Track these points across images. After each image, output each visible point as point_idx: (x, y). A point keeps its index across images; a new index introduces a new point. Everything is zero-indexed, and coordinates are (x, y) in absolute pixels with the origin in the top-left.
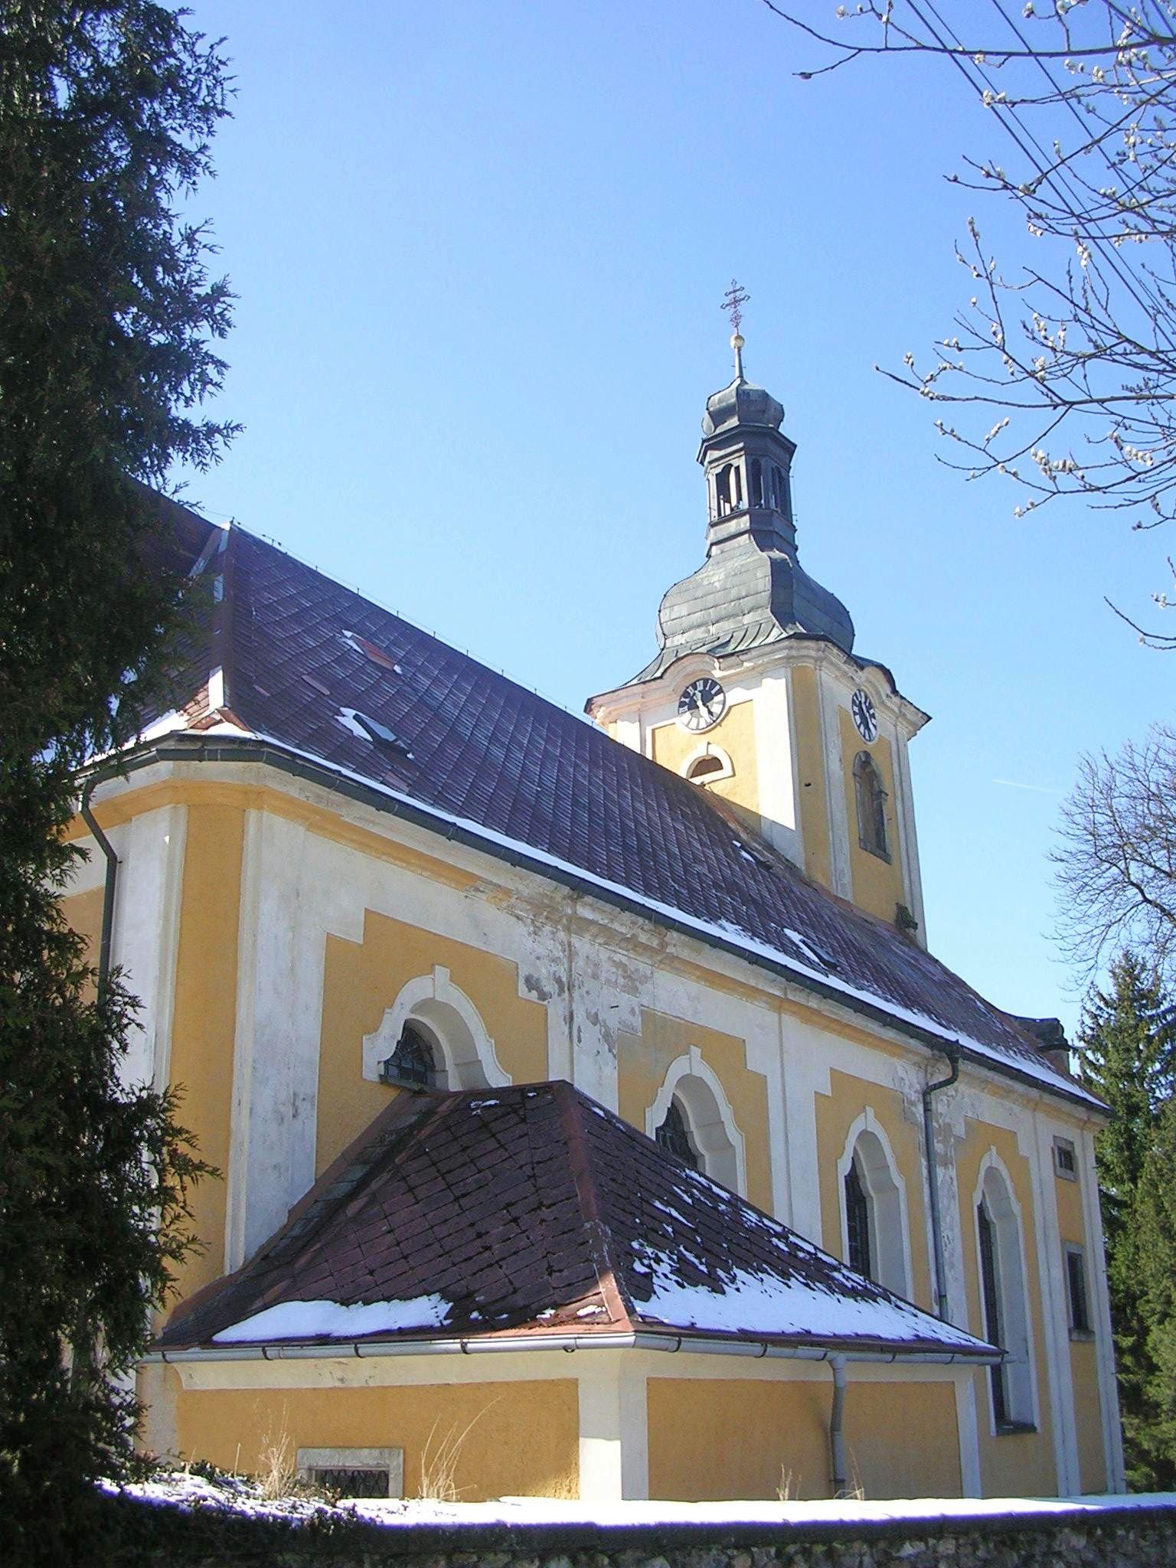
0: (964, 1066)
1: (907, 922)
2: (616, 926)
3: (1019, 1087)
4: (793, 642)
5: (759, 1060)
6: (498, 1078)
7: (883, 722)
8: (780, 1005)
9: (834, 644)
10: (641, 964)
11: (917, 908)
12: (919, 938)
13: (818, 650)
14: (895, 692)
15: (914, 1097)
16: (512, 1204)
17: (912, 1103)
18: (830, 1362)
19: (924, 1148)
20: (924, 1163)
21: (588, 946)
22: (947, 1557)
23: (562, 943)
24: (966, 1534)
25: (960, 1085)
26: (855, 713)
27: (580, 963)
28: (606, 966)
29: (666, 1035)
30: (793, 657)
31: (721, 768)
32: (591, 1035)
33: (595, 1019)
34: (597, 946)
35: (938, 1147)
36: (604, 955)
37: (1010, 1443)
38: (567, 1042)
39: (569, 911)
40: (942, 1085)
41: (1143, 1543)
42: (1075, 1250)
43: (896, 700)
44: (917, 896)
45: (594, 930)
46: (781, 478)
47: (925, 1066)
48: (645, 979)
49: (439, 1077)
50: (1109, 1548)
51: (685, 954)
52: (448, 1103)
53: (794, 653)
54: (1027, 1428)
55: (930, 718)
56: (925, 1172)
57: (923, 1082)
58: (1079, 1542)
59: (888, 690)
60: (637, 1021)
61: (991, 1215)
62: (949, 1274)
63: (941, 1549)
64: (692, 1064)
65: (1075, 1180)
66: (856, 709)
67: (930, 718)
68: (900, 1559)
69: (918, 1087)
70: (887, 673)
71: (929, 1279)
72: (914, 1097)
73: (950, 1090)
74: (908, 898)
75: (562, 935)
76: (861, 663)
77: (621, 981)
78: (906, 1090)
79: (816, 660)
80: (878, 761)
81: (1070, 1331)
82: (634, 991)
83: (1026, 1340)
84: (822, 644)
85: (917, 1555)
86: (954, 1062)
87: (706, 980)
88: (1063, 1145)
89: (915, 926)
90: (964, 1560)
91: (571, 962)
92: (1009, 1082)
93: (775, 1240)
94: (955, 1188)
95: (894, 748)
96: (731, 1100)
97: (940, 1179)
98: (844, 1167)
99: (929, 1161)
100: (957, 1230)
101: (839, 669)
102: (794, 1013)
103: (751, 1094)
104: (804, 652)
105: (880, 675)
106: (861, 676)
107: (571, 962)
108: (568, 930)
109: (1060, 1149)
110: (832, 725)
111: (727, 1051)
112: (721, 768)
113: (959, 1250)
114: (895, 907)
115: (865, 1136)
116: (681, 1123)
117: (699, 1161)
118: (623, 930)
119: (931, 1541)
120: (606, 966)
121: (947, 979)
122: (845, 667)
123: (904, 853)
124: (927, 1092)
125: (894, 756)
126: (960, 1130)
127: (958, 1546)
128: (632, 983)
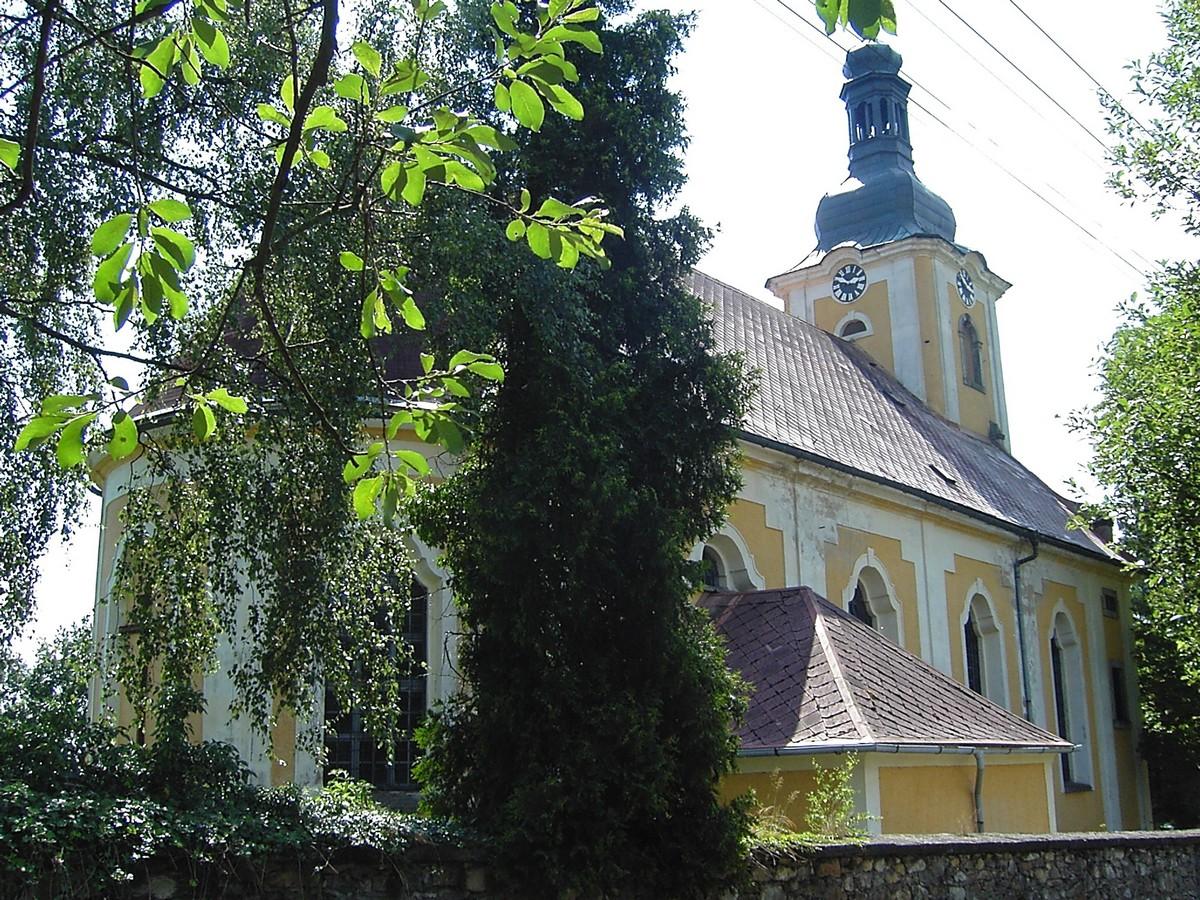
0: (1041, 546)
1: (996, 436)
2: (822, 477)
3: (1078, 557)
4: (915, 240)
5: (909, 553)
6: (760, 586)
7: (978, 294)
8: (921, 516)
9: (944, 240)
10: (835, 499)
11: (1004, 424)
12: (1006, 446)
13: (933, 245)
14: (987, 270)
15: (1008, 569)
16: (787, 666)
17: (1007, 573)
18: (975, 755)
19: (1015, 603)
20: (1015, 612)
21: (805, 490)
22: (1051, 861)
23: (790, 490)
24: (1059, 850)
25: (1038, 559)
26: (959, 287)
27: (801, 501)
28: (815, 501)
29: (851, 541)
30: (915, 250)
31: (865, 329)
32: (809, 548)
33: (810, 537)
34: (810, 490)
35: (1024, 601)
36: (815, 494)
37: (1073, 798)
38: (795, 553)
39: (794, 470)
40: (1026, 560)
41: (1156, 857)
42: (1118, 666)
43: (987, 274)
44: (1003, 415)
45: (809, 480)
46: (901, 109)
47: (1015, 547)
48: (839, 507)
49: (721, 580)
50: (1137, 860)
51: (863, 490)
52: (734, 600)
53: (914, 247)
54: (1088, 788)
55: (1011, 285)
56: (1016, 619)
57: (1014, 559)
58: (1120, 855)
59: (982, 269)
60: (835, 535)
61: (1060, 643)
62: (1032, 686)
63: (1047, 857)
64: (869, 559)
65: (1118, 618)
66: (959, 284)
67: (1011, 285)
68: (1027, 862)
69: (1011, 562)
70: (980, 256)
71: (1020, 688)
72: (1008, 569)
73: (1032, 563)
74: (997, 416)
75: (790, 485)
76: (961, 251)
77: (826, 510)
78: (1003, 565)
79: (931, 251)
80: (975, 321)
81: (1114, 721)
82: (832, 515)
83: (1084, 729)
84: (936, 240)
85: (1036, 860)
86: (1035, 545)
87: (876, 504)
88: (1110, 594)
89: (1003, 437)
90: (1058, 863)
91: (795, 502)
92: (1072, 554)
93: (410, 292)
94: (1036, 629)
95: (987, 309)
96: (892, 580)
97: (1026, 622)
98: (964, 620)
99: (1019, 611)
100: (1038, 657)
101: (947, 257)
102: (930, 520)
103: (906, 572)
104: (923, 247)
105: (977, 257)
106: (963, 261)
107: (795, 502)
108: (793, 481)
109: (1107, 596)
110: (943, 294)
111: (889, 547)
112: (865, 329)
113: (1039, 670)
114: (988, 424)
115: (978, 598)
116: (861, 597)
117: (873, 620)
118: (827, 479)
119: (1042, 853)
120: (815, 501)
121: (1028, 477)
122: (951, 255)
123: (994, 386)
124: (1018, 564)
125: (987, 313)
126: (1038, 588)
127: (1055, 856)
128: (832, 510)
